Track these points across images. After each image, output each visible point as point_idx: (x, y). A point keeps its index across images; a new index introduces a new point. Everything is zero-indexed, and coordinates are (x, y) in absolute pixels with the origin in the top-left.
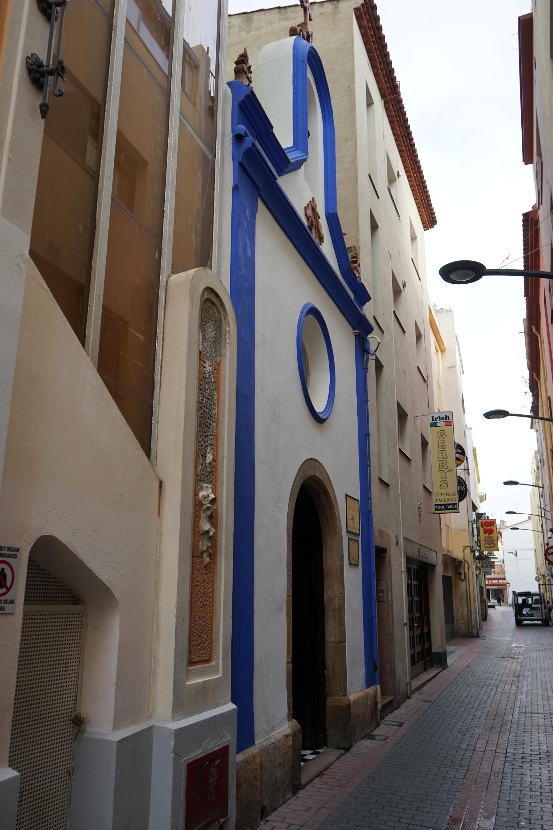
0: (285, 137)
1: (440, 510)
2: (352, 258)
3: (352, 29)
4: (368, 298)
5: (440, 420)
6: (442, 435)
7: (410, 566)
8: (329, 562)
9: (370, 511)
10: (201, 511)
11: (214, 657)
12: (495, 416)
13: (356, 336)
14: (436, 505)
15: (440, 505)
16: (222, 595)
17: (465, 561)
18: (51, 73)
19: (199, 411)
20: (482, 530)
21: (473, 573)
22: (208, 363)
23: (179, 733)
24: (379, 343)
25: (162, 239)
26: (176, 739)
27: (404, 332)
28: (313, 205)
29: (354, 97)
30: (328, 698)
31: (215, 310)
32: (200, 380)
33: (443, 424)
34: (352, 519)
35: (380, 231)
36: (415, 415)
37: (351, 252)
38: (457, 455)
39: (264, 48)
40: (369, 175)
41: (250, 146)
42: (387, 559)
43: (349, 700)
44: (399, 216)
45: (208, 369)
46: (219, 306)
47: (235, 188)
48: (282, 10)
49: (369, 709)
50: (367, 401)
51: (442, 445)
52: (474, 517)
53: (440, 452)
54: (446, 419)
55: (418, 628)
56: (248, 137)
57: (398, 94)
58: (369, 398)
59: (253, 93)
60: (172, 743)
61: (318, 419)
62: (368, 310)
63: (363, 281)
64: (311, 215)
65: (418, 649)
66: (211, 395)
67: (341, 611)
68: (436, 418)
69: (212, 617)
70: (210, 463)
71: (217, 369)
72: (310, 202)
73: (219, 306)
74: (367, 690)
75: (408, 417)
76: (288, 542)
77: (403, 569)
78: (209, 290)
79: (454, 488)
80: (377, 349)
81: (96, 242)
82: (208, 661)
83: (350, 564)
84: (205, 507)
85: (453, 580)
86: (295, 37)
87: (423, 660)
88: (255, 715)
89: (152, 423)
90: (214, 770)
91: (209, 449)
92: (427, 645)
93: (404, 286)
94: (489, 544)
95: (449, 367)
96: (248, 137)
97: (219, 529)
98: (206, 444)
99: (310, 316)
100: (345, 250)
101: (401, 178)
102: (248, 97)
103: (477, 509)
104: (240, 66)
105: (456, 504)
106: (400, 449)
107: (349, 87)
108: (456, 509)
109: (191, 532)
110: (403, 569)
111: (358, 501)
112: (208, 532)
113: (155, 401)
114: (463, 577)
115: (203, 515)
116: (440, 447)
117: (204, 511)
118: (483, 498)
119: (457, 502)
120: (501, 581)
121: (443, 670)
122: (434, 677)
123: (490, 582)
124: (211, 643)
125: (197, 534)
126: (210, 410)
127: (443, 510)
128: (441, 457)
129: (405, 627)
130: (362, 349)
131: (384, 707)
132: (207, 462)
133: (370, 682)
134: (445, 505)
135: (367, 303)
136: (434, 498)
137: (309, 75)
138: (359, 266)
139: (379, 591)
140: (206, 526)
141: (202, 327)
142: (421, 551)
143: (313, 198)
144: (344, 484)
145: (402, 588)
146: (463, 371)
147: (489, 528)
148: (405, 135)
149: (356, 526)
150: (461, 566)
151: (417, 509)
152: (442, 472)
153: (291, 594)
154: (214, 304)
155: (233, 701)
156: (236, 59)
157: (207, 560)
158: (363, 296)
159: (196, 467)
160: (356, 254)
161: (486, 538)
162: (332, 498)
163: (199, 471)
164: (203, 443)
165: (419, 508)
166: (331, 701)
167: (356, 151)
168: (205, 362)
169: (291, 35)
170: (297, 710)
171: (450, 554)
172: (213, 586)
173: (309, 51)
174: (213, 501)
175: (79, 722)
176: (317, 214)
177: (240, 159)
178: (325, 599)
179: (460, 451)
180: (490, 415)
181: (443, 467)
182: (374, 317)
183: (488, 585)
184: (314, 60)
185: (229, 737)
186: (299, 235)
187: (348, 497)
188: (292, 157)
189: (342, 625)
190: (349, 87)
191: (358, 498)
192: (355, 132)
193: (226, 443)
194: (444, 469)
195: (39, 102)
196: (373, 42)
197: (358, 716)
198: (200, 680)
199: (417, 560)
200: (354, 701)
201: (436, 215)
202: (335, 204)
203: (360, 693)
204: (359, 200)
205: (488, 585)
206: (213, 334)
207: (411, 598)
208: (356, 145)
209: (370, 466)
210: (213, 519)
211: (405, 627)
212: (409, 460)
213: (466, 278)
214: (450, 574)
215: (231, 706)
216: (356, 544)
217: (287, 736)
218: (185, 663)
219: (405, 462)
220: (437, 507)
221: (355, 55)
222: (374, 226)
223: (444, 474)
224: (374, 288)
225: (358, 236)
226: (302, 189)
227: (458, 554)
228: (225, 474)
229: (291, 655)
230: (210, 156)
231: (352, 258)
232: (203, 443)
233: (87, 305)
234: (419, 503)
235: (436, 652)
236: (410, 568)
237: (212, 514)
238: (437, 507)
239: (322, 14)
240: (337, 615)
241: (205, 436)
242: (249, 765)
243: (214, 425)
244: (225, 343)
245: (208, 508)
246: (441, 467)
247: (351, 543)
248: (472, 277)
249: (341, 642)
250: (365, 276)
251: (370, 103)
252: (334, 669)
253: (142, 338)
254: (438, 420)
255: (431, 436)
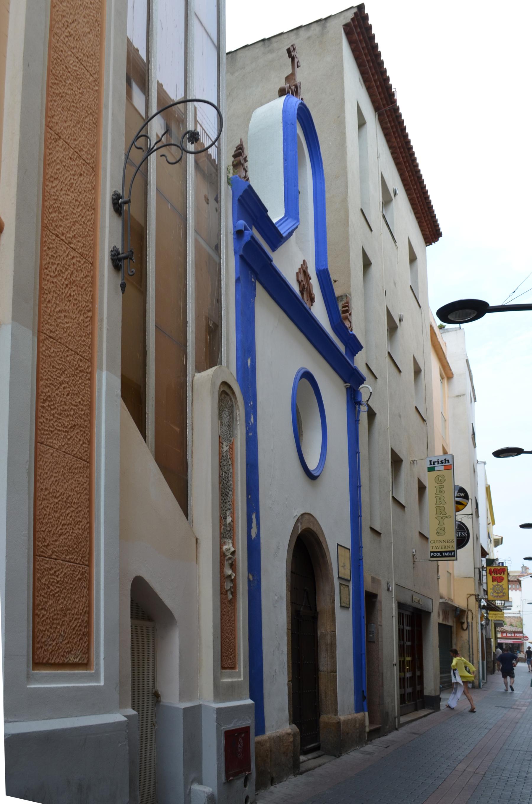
0: (276, 213)
1: (436, 557)
2: (343, 307)
3: (341, 50)
4: (359, 347)
5: (438, 463)
6: (440, 480)
7: (402, 611)
8: (322, 604)
9: (361, 559)
10: (225, 560)
11: (237, 666)
12: (506, 454)
13: (347, 389)
14: (431, 552)
15: (436, 552)
16: (241, 623)
17: (468, 610)
18: (125, 258)
19: (220, 483)
20: (490, 578)
21: (477, 623)
22: (225, 444)
23: (219, 711)
24: (371, 393)
25: (187, 346)
26: (217, 713)
27: (400, 371)
28: (304, 268)
29: (344, 128)
30: (322, 716)
31: (228, 399)
32: (220, 459)
33: (442, 468)
34: (343, 567)
35: (374, 268)
36: (411, 459)
37: (342, 301)
38: (457, 499)
39: (254, 115)
40: (362, 210)
41: (249, 238)
42: (378, 604)
43: (340, 719)
44: (395, 241)
45: (225, 448)
46: (231, 395)
47: (238, 280)
48: (266, 42)
49: (358, 730)
50: (358, 453)
51: (441, 490)
52: (484, 564)
53: (438, 498)
54: (445, 463)
55: (410, 671)
56: (248, 230)
57: (394, 102)
58: (361, 450)
59: (250, 187)
60: (215, 716)
61: (311, 476)
62: (359, 362)
63: (354, 332)
64: (303, 279)
65: (409, 690)
66: (228, 470)
67: (333, 646)
68: (434, 462)
69: (235, 638)
70: (229, 524)
71: (231, 448)
72: (302, 265)
73: (231, 395)
74: (356, 715)
75: (404, 463)
76: (287, 585)
77: (394, 614)
78: (225, 383)
79: (451, 535)
80: (369, 398)
81: (147, 364)
82: (233, 668)
83: (341, 606)
84: (227, 557)
85: (454, 629)
86: (284, 97)
87: (413, 701)
88: (265, 715)
89: (187, 495)
90: (240, 740)
91: (228, 513)
92: (418, 688)
93: (401, 320)
94: (498, 593)
95: (457, 396)
96: (248, 230)
97: (237, 574)
98: (226, 509)
99: (305, 380)
100: (335, 300)
101: (398, 197)
102: (246, 191)
103: (488, 554)
104: (238, 159)
105: (454, 551)
106: (393, 497)
107: (338, 117)
108: (454, 556)
109: (219, 576)
110: (394, 614)
111: (349, 549)
112: (230, 576)
113: (189, 478)
114: (465, 626)
115: (226, 564)
116: (438, 492)
117: (227, 560)
118: (498, 542)
119: (455, 549)
120: (518, 635)
121: (434, 712)
122: (425, 716)
123: (505, 635)
124: (235, 656)
125: (224, 578)
126: (228, 482)
127: (439, 557)
128: (438, 503)
129: (395, 667)
130: (353, 399)
131: (371, 732)
132: (228, 523)
133: (359, 708)
134: (441, 552)
135: (359, 353)
136: (430, 545)
137: (299, 131)
138: (350, 314)
139: (368, 632)
140: (229, 572)
141: (220, 416)
142: (414, 597)
143: (304, 261)
144: (336, 534)
145: (393, 631)
146: (475, 399)
147: (499, 575)
148: (402, 145)
149: (347, 572)
150: (464, 615)
151: (411, 557)
152: (439, 519)
153: (290, 628)
154: (227, 394)
155: (251, 698)
156: (233, 153)
157: (230, 596)
158: (354, 346)
159: (220, 528)
160: (347, 303)
161: (495, 586)
162: (324, 547)
163: (222, 530)
164: (224, 508)
165: (413, 555)
166: (325, 718)
167: (347, 188)
168: (223, 444)
169: (280, 96)
170: (296, 716)
171: (450, 602)
172: (235, 615)
173: (299, 108)
174: (233, 553)
175: (157, 696)
176: (308, 275)
177: (241, 253)
178: (319, 635)
179: (463, 495)
180: (498, 454)
181: (440, 511)
182: (367, 364)
183: (500, 638)
184: (304, 116)
185: (249, 721)
186: (294, 308)
187: (339, 547)
188: (283, 230)
189: (333, 657)
190: (338, 117)
191: (349, 547)
192: (346, 167)
193: (240, 507)
194: (442, 516)
195: (120, 282)
196: (365, 54)
197: (347, 734)
198: (230, 680)
199: (409, 606)
200: (344, 721)
201: (440, 226)
202: (326, 260)
203: (350, 716)
204: (350, 242)
205: (500, 638)
206: (227, 419)
207: (402, 642)
208: (347, 182)
209: (361, 516)
210: (233, 566)
211: (395, 667)
212: (403, 507)
213: (467, 317)
214: (450, 623)
215: (250, 702)
216: (347, 589)
217: (289, 734)
218: (220, 667)
219: (398, 510)
220: (432, 554)
221: (345, 78)
222: (367, 264)
223: (441, 520)
224: (367, 332)
225: (349, 281)
226: (292, 260)
227: (460, 602)
228: (240, 532)
229: (291, 675)
230: (216, 258)
231: (343, 307)
232: (224, 508)
233: (145, 413)
234: (414, 550)
235: (427, 694)
236: (403, 614)
237: (232, 562)
238: (432, 554)
239: (309, 38)
240: (329, 649)
241: (225, 503)
242: (262, 746)
243: (231, 493)
244: (237, 425)
245: (230, 558)
246: (439, 513)
247: (342, 588)
248: (474, 315)
249: (332, 672)
250: (357, 329)
251: (362, 123)
252: (326, 693)
253: (178, 429)
254: (436, 463)
255: (428, 480)
